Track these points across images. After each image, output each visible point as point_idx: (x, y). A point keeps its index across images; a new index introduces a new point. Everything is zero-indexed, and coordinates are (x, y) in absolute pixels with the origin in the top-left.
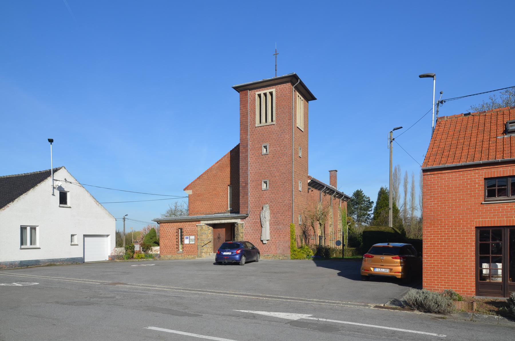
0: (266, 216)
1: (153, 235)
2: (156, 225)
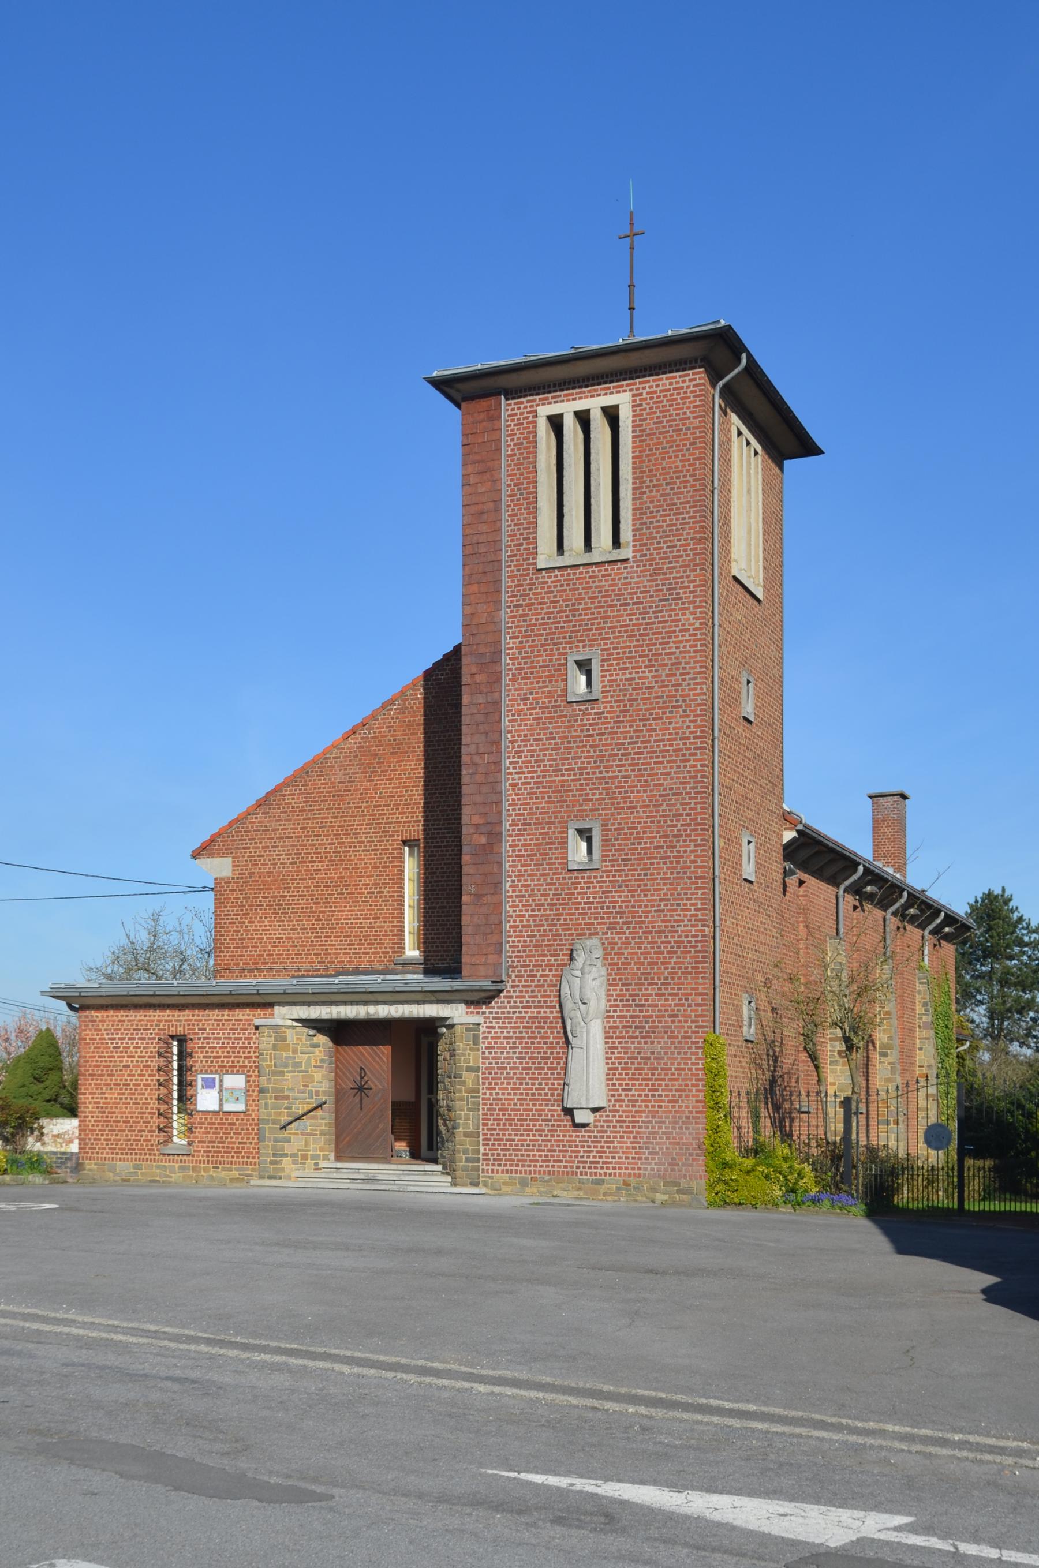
0: (590, 995)
1: (45, 1061)
2: (60, 1017)
